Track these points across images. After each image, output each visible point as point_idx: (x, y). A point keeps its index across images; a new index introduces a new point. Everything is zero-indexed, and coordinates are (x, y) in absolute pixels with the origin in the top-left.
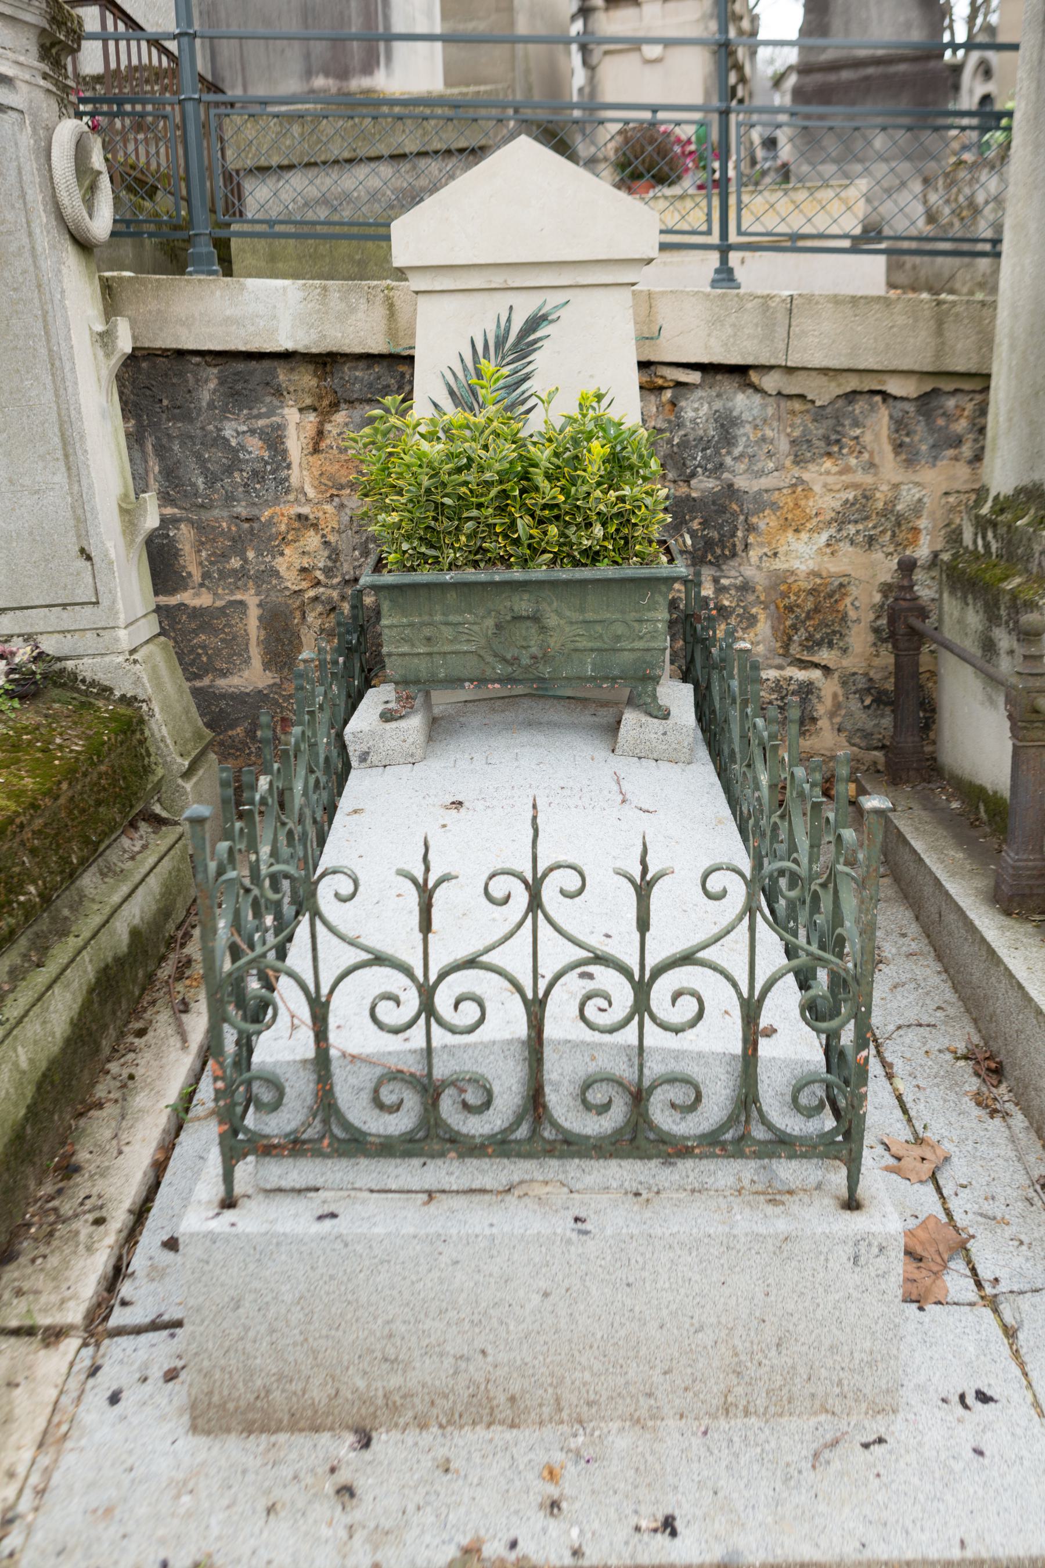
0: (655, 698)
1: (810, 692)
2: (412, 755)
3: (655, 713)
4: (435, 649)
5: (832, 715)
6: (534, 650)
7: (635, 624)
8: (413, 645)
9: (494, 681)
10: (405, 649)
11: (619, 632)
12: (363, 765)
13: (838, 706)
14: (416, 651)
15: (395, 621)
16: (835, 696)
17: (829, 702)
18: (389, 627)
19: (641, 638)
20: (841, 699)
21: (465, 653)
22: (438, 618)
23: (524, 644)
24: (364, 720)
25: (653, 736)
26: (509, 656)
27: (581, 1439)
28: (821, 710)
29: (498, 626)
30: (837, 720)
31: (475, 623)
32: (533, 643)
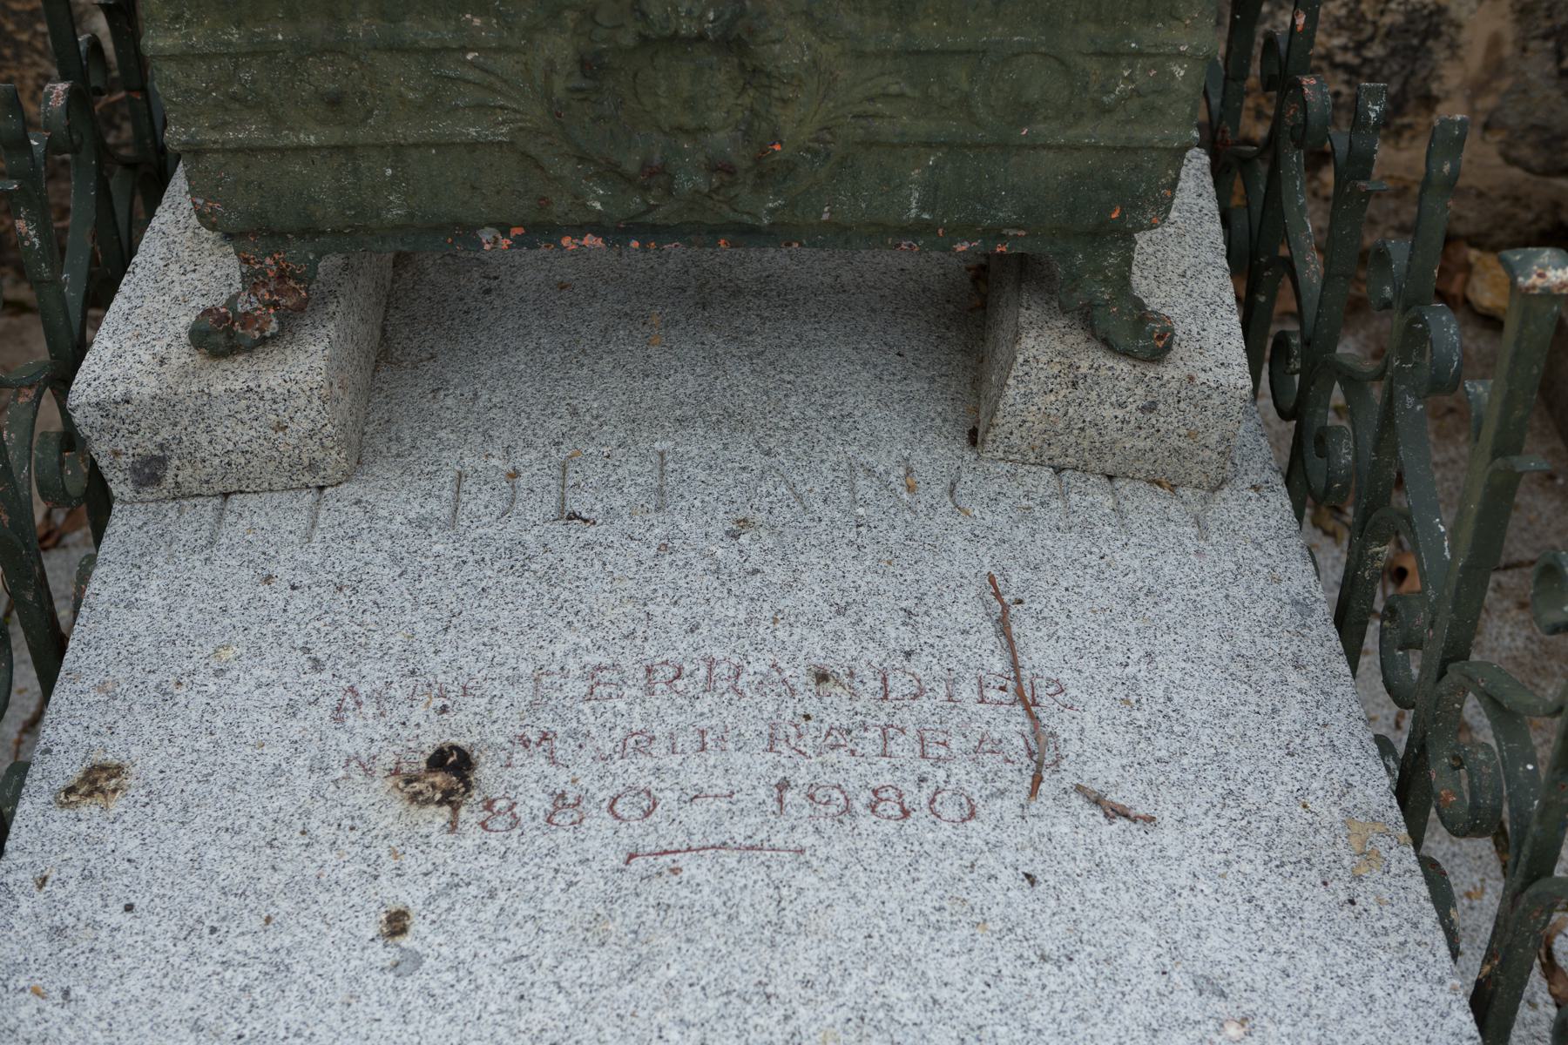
0: (1123, 282)
1: (1433, 32)
2: (312, 467)
3: (1124, 341)
4: (362, 135)
5: (1478, 89)
6: (722, 140)
7: (1094, 66)
8: (277, 122)
9: (579, 230)
10: (251, 131)
11: (1033, 94)
12: (148, 493)
13: (1495, 67)
14: (289, 138)
15: (198, 39)
16: (1495, 42)
17: (1475, 58)
18: (184, 58)
19: (1105, 110)
20: (1508, 50)
21: (473, 146)
22: (361, 27)
23: (688, 120)
24: (133, 353)
25: (1108, 412)
26: (632, 164)
27: (744, 960)
28: (1452, 77)
29: (590, 65)
30: (1487, 102)
31: (503, 49)
32: (717, 116)
